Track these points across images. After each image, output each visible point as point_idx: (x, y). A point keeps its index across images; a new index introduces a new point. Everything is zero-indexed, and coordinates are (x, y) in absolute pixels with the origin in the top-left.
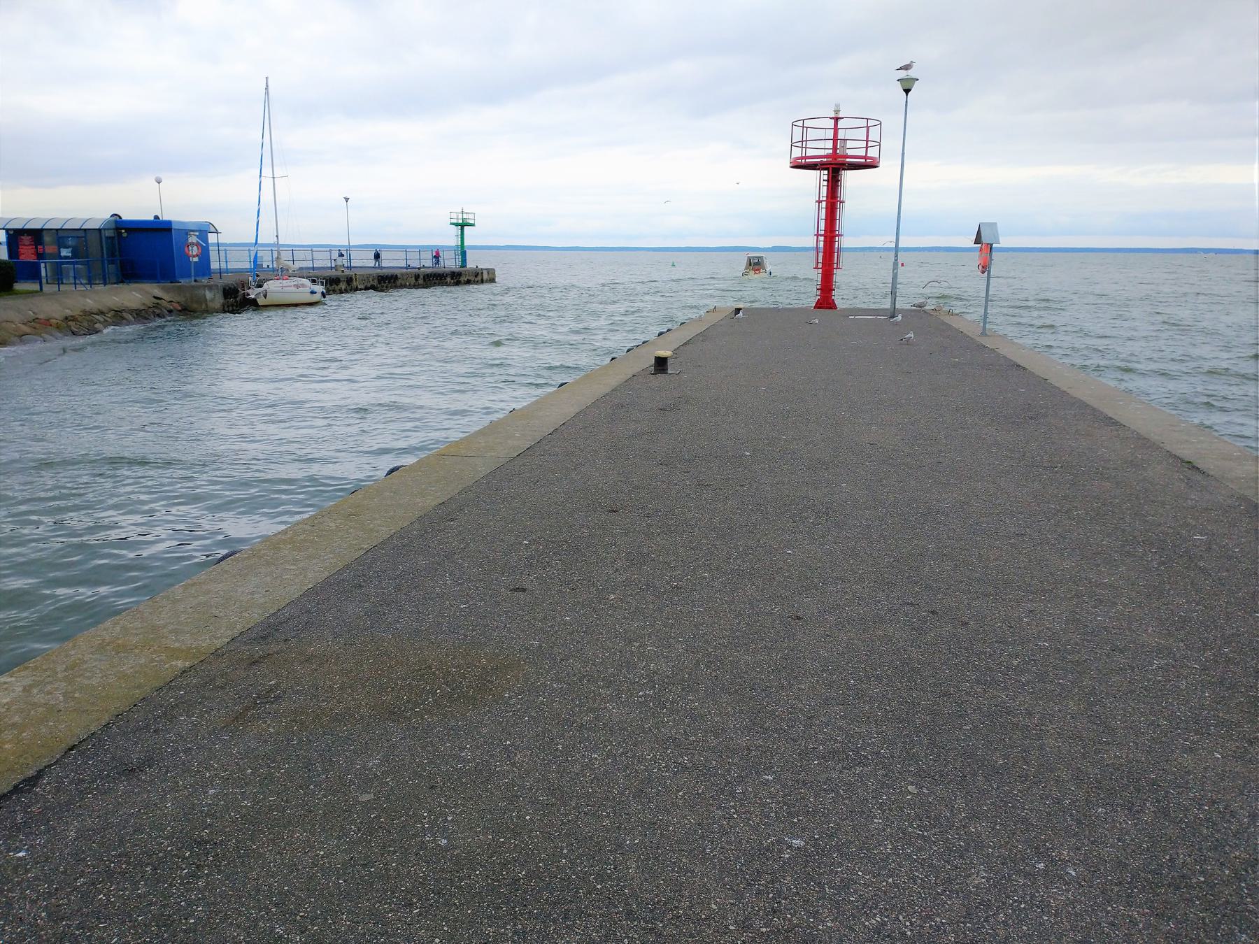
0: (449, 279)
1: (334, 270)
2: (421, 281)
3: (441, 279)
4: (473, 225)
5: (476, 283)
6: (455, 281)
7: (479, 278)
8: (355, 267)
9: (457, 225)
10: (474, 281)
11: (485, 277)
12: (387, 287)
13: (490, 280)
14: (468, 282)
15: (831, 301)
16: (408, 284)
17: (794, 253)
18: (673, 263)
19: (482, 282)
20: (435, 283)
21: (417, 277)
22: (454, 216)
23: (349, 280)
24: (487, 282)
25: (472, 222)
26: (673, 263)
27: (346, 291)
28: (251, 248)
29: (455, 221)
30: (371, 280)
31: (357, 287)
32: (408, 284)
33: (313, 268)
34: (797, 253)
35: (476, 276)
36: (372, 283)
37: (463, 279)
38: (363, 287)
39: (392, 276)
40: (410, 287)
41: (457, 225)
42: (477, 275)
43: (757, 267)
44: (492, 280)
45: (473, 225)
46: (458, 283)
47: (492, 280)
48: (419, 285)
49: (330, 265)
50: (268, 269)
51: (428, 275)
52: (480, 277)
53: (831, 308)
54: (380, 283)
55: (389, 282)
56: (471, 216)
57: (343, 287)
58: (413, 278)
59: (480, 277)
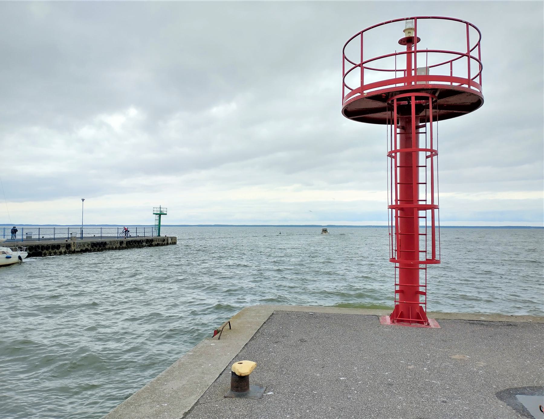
0: (144, 244)
1: (70, 240)
2: (124, 245)
3: (104, 246)
4: (166, 214)
5: (164, 245)
6: (149, 244)
7: (166, 242)
8: (85, 237)
9: (156, 214)
10: (162, 244)
11: (170, 241)
12: (137, 246)
13: (173, 243)
14: (158, 245)
15: (418, 310)
16: (114, 247)
17: (337, 228)
18: (280, 232)
19: (168, 244)
20: (134, 246)
21: (121, 243)
22: (155, 209)
23: (68, 246)
24: (170, 244)
25: (165, 213)
26: (280, 232)
27: (65, 253)
28: (153, 227)
29: (155, 212)
30: (86, 245)
31: (74, 250)
32: (114, 247)
33: (54, 239)
34: (52, 237)
35: (163, 241)
36: (86, 247)
37: (107, 247)
38: (79, 250)
39: (140, 241)
40: (116, 249)
41: (156, 214)
42: (164, 240)
43: (325, 231)
44: (175, 243)
45: (166, 214)
46: (151, 246)
47: (175, 243)
48: (123, 247)
49: (38, 237)
50: (43, 239)
51: (129, 242)
52: (171, 242)
53: (422, 323)
54: (92, 247)
55: (100, 247)
56: (165, 210)
57: (63, 251)
58: (119, 244)
59: (164, 242)
